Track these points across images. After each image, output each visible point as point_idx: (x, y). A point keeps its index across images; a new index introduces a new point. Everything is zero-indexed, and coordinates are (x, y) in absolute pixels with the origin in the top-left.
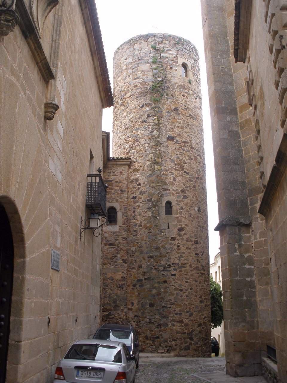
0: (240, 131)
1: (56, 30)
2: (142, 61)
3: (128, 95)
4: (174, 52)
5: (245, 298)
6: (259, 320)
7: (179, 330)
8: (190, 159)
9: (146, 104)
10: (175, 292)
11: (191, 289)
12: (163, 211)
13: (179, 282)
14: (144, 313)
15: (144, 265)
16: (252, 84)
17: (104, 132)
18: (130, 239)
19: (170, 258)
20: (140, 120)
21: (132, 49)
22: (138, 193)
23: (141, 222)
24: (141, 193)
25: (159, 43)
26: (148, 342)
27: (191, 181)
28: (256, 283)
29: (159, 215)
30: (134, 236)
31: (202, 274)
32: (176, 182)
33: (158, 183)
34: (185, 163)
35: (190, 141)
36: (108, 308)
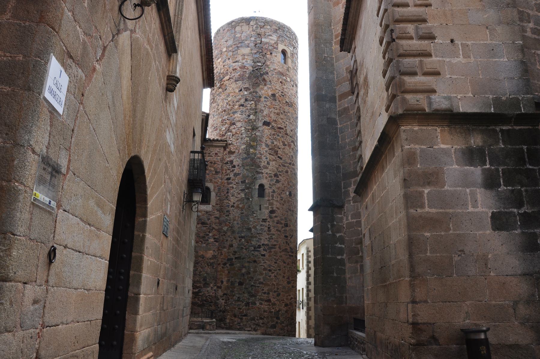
0: (337, 118)
1: (179, 5)
2: (243, 44)
3: (227, 78)
4: (274, 37)
5: (335, 275)
6: (348, 296)
7: (266, 309)
8: (284, 145)
9: (244, 88)
10: (264, 272)
11: (279, 270)
12: (256, 194)
13: (268, 263)
14: (232, 291)
15: (235, 245)
16: (356, 73)
17: (204, 113)
18: (222, 219)
19: (261, 239)
20: (238, 103)
21: (233, 31)
22: (232, 176)
23: (234, 203)
24: (236, 175)
25: (261, 28)
26: (236, 319)
27: (284, 166)
28: (346, 261)
29: (252, 197)
30: (226, 216)
31: (290, 255)
32: (269, 166)
33: (252, 166)
34: (279, 149)
35: (285, 127)
36: (198, 285)
